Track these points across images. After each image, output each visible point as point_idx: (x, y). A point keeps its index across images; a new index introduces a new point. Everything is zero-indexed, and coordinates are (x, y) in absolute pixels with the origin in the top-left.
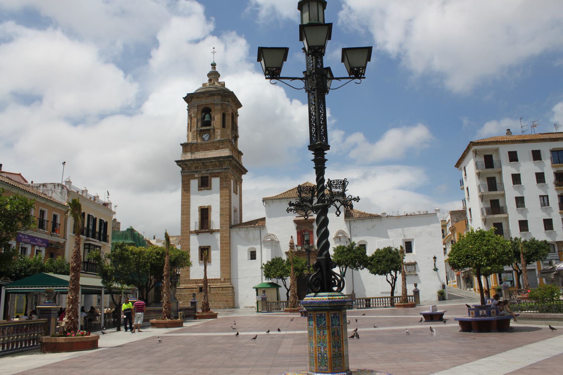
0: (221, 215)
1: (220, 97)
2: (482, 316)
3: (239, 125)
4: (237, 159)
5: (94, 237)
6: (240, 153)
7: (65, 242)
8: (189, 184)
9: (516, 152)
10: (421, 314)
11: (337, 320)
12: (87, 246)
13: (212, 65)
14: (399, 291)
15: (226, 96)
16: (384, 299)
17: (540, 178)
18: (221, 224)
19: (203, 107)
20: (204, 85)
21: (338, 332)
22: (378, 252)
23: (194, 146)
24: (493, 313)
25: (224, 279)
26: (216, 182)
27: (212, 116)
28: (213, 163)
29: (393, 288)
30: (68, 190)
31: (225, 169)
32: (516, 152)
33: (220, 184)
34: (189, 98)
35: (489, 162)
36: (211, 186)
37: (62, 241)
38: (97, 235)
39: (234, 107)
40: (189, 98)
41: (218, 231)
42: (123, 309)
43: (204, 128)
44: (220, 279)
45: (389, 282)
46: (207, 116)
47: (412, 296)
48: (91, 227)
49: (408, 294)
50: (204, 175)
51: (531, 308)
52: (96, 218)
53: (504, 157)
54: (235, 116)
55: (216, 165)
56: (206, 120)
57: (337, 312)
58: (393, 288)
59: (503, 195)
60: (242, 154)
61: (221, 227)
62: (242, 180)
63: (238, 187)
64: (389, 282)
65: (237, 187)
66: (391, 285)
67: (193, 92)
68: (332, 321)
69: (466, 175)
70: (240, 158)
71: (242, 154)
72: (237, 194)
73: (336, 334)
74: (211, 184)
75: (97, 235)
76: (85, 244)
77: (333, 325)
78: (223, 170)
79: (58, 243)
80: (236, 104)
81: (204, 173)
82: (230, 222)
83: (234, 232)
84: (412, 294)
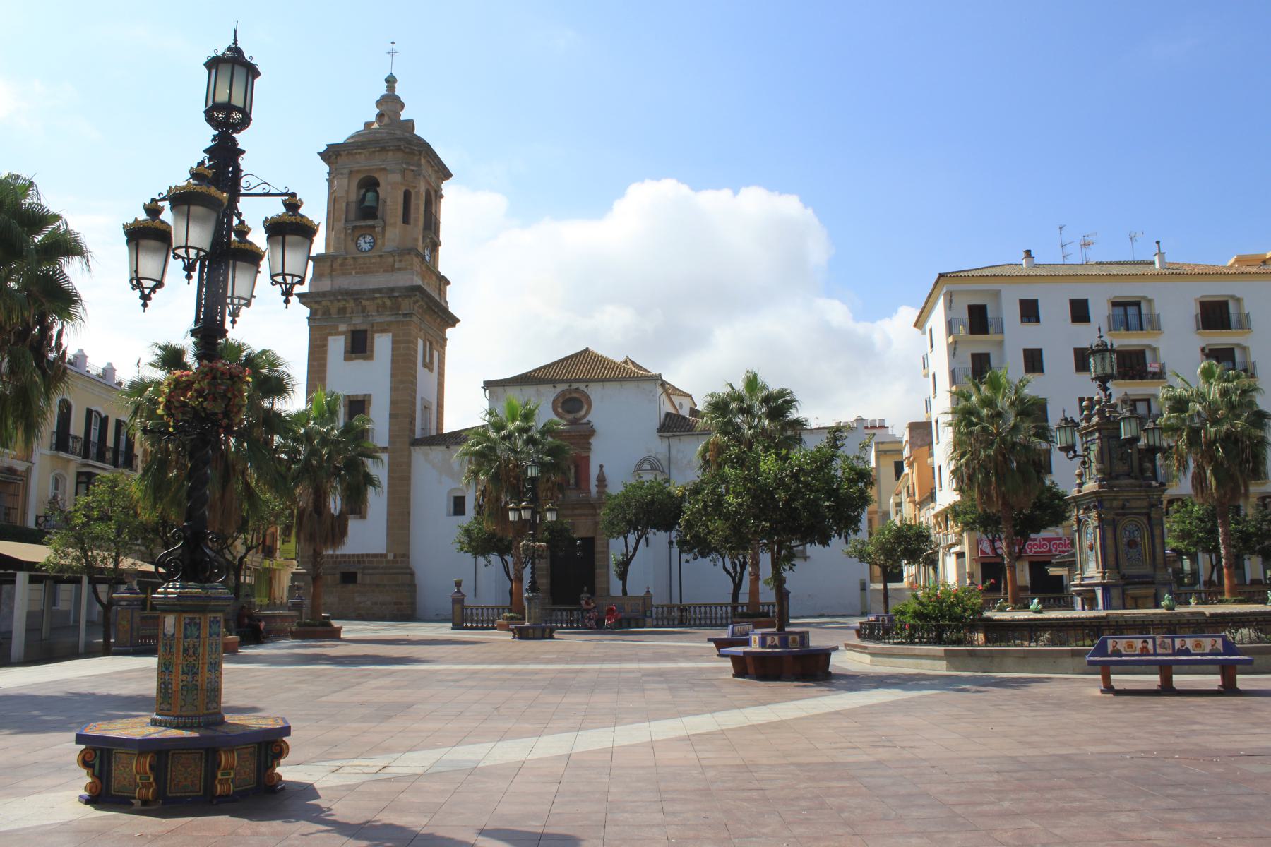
0: (392, 416)
1: (400, 155)
2: (770, 647)
3: (442, 220)
4: (435, 295)
5: (101, 457)
6: (444, 282)
7: (28, 471)
8: (325, 345)
9: (1036, 301)
10: (709, 640)
11: (194, 629)
12: (84, 479)
13: (387, 81)
14: (744, 598)
15: (412, 153)
18: (390, 437)
19: (362, 176)
20: (368, 125)
21: (196, 649)
23: (339, 262)
24: (794, 641)
25: (395, 556)
26: (382, 344)
27: (381, 196)
28: (379, 301)
29: (737, 587)
31: (405, 315)
32: (1036, 301)
33: (393, 349)
34: (331, 154)
35: (978, 319)
36: (372, 351)
37: (20, 466)
38: (109, 455)
39: (433, 179)
40: (331, 154)
41: (384, 449)
42: (760, 650)
43: (362, 223)
44: (385, 556)
45: (728, 572)
46: (370, 195)
48: (94, 436)
49: (762, 600)
50: (358, 328)
52: (107, 417)
53: (1011, 313)
54: (434, 197)
55: (384, 306)
56: (366, 204)
57: (197, 616)
58: (737, 587)
59: (1000, 344)
60: (448, 283)
61: (390, 442)
62: (445, 340)
63: (436, 354)
64: (728, 572)
65: (431, 356)
66: (734, 579)
67: (341, 141)
68: (185, 629)
70: (442, 293)
71: (448, 283)
72: (431, 370)
73: (191, 651)
74: (372, 346)
75: (109, 455)
76: (79, 474)
77: (186, 637)
78: (400, 318)
79: (11, 471)
80: (437, 172)
81: (358, 322)
82: (413, 431)
83: (418, 454)
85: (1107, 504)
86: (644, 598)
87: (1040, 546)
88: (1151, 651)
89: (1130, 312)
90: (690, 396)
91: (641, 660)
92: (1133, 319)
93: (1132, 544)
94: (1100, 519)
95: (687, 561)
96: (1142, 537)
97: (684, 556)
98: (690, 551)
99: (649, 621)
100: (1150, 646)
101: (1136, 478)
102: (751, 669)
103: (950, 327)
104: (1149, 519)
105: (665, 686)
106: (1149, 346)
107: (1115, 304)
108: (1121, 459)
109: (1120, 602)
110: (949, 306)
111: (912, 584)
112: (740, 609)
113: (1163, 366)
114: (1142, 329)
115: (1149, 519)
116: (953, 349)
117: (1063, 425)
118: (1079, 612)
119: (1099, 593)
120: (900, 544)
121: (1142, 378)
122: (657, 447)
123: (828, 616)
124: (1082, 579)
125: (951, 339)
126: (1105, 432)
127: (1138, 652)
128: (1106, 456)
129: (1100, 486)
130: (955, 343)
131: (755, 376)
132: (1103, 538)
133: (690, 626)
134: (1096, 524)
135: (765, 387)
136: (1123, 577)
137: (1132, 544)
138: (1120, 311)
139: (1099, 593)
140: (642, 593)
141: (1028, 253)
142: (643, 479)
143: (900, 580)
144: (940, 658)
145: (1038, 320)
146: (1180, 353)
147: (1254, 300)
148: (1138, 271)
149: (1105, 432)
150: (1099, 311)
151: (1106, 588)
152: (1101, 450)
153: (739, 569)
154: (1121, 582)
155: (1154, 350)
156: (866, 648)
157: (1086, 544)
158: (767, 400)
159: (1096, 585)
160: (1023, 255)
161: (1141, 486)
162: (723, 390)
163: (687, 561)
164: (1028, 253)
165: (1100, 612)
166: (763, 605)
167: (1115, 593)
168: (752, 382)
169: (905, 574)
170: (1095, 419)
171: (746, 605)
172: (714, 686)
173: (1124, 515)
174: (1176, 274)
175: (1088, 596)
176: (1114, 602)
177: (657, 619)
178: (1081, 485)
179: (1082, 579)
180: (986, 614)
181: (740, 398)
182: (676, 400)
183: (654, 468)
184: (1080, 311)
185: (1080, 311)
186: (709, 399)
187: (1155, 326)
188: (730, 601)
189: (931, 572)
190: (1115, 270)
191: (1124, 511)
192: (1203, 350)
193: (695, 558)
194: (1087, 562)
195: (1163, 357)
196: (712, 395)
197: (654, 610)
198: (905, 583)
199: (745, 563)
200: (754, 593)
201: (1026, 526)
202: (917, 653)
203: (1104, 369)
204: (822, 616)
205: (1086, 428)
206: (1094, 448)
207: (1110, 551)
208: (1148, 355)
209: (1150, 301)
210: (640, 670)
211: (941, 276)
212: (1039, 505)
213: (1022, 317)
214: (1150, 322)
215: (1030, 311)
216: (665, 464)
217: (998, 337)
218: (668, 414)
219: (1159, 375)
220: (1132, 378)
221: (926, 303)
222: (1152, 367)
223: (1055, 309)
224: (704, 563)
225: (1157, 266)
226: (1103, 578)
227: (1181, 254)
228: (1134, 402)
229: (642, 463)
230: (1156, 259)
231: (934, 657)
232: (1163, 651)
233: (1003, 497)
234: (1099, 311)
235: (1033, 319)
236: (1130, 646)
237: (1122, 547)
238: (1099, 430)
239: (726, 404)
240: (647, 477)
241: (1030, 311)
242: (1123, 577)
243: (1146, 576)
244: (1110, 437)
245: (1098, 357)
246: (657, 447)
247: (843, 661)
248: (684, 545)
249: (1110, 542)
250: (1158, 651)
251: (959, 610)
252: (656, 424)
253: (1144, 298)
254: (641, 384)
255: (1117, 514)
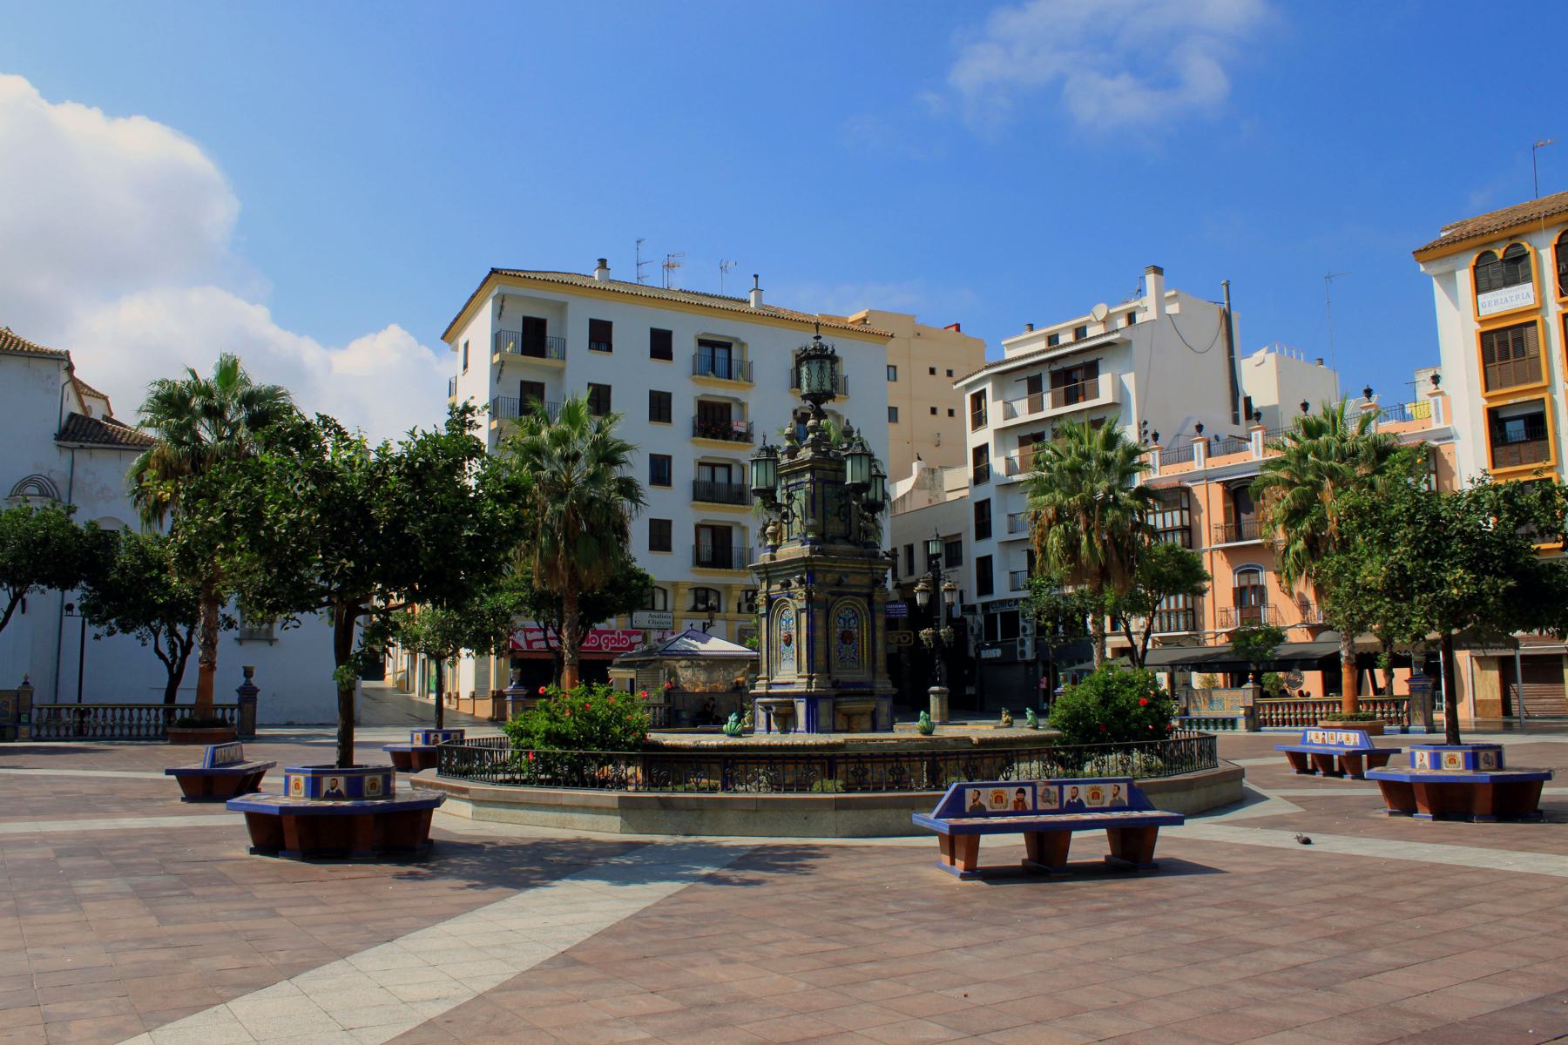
2: (329, 796)
10: (168, 772)
14: (186, 694)
16: (135, 713)
17: (660, 407)
22: (92, 525)
24: (373, 786)
30: (1244, 980)
35: (534, 337)
42: (310, 803)
45: (162, 656)
47: (232, 707)
49: (216, 700)
51: (1123, 907)
53: (577, 335)
58: (175, 679)
59: (560, 372)
64: (162, 656)
66: (170, 667)
69: (465, 367)
84: (234, 699)
85: (819, 578)
86: (18, 694)
87: (619, 641)
88: (1030, 807)
89: (718, 355)
90: (105, 398)
91: (37, 813)
92: (721, 365)
93: (846, 637)
94: (809, 598)
95: (97, 637)
96: (860, 628)
97: (92, 630)
98: (102, 621)
99: (24, 729)
100: (1028, 799)
101: (855, 543)
102: (291, 839)
103: (497, 343)
104: (871, 603)
105: (120, 884)
106: (736, 400)
107: (702, 343)
108: (838, 515)
109: (829, 721)
110: (499, 314)
111: (400, 682)
112: (178, 713)
113: (750, 426)
114: (730, 377)
115: (871, 603)
116: (498, 372)
117: (764, 456)
118: (764, 737)
119: (801, 708)
120: (469, 624)
121: (726, 437)
122: (54, 462)
123: (300, 726)
124: (769, 686)
125: (497, 358)
126: (819, 474)
127: (1010, 808)
128: (819, 507)
129: (812, 551)
130: (502, 363)
131: (235, 364)
132: (811, 628)
133: (94, 738)
134: (803, 605)
135: (246, 382)
136: (835, 684)
137: (846, 637)
138: (707, 351)
139: (801, 708)
140: (16, 685)
141: (603, 262)
142: (31, 505)
143: (380, 675)
144: (608, 811)
145: (610, 349)
146: (769, 409)
147: (855, 362)
148: (733, 308)
149: (819, 474)
150: (684, 347)
151: (812, 700)
152: (812, 499)
153: (179, 653)
154: (833, 692)
155: (742, 405)
156: (465, 791)
157: (779, 634)
158: (249, 399)
159: (798, 695)
160: (597, 264)
161: (862, 555)
162: (181, 378)
163: (97, 637)
164: (603, 262)
165: (801, 737)
166: (216, 707)
167: (824, 707)
168: (228, 371)
169: (388, 670)
170: (806, 454)
171: (191, 707)
172: (224, 880)
173: (841, 594)
174: (775, 317)
175: (783, 710)
176: (824, 721)
177: (39, 728)
178: (774, 548)
179: (769, 686)
180: (653, 736)
181: (207, 392)
182: (87, 401)
183: (43, 493)
184: (661, 345)
185: (661, 345)
186: (156, 388)
187: (746, 374)
188: (161, 700)
189: (433, 667)
190: (707, 302)
191: (839, 589)
192: (795, 412)
193: (111, 633)
194: (779, 661)
195: (753, 413)
196: (161, 384)
197: (35, 712)
198: (389, 681)
199: (190, 643)
200: (205, 689)
201: (593, 609)
202: (565, 802)
203: (821, 383)
204: (290, 725)
205: (790, 466)
206: (800, 496)
207: (820, 646)
208: (735, 410)
209: (742, 345)
210: (45, 839)
211: (494, 271)
212: (613, 585)
213: (591, 341)
214: (741, 370)
215: (601, 335)
216: (63, 488)
217: (558, 364)
218: (73, 416)
219: (745, 437)
220: (714, 436)
221: (465, 308)
222: (739, 427)
223: (631, 337)
224: (127, 642)
225: (752, 305)
226: (809, 685)
227: (778, 297)
228: (713, 466)
229: (25, 483)
230: (752, 297)
231: (598, 810)
232: (1047, 806)
233: (572, 569)
234: (684, 347)
235: (603, 346)
236: (999, 799)
237: (835, 641)
238: (812, 470)
239: (185, 401)
240: (36, 504)
241: (601, 335)
242: (835, 684)
243: (861, 684)
244: (825, 482)
245: (815, 366)
246: (54, 462)
247: (455, 819)
248: (92, 612)
249: (820, 633)
250: (1040, 806)
251: (618, 730)
252: (54, 428)
253: (737, 340)
254: (34, 362)
255: (833, 594)
